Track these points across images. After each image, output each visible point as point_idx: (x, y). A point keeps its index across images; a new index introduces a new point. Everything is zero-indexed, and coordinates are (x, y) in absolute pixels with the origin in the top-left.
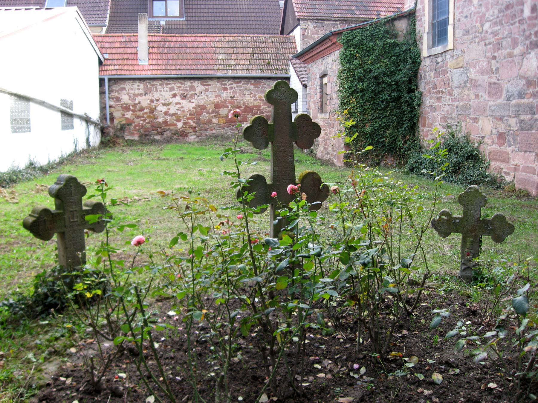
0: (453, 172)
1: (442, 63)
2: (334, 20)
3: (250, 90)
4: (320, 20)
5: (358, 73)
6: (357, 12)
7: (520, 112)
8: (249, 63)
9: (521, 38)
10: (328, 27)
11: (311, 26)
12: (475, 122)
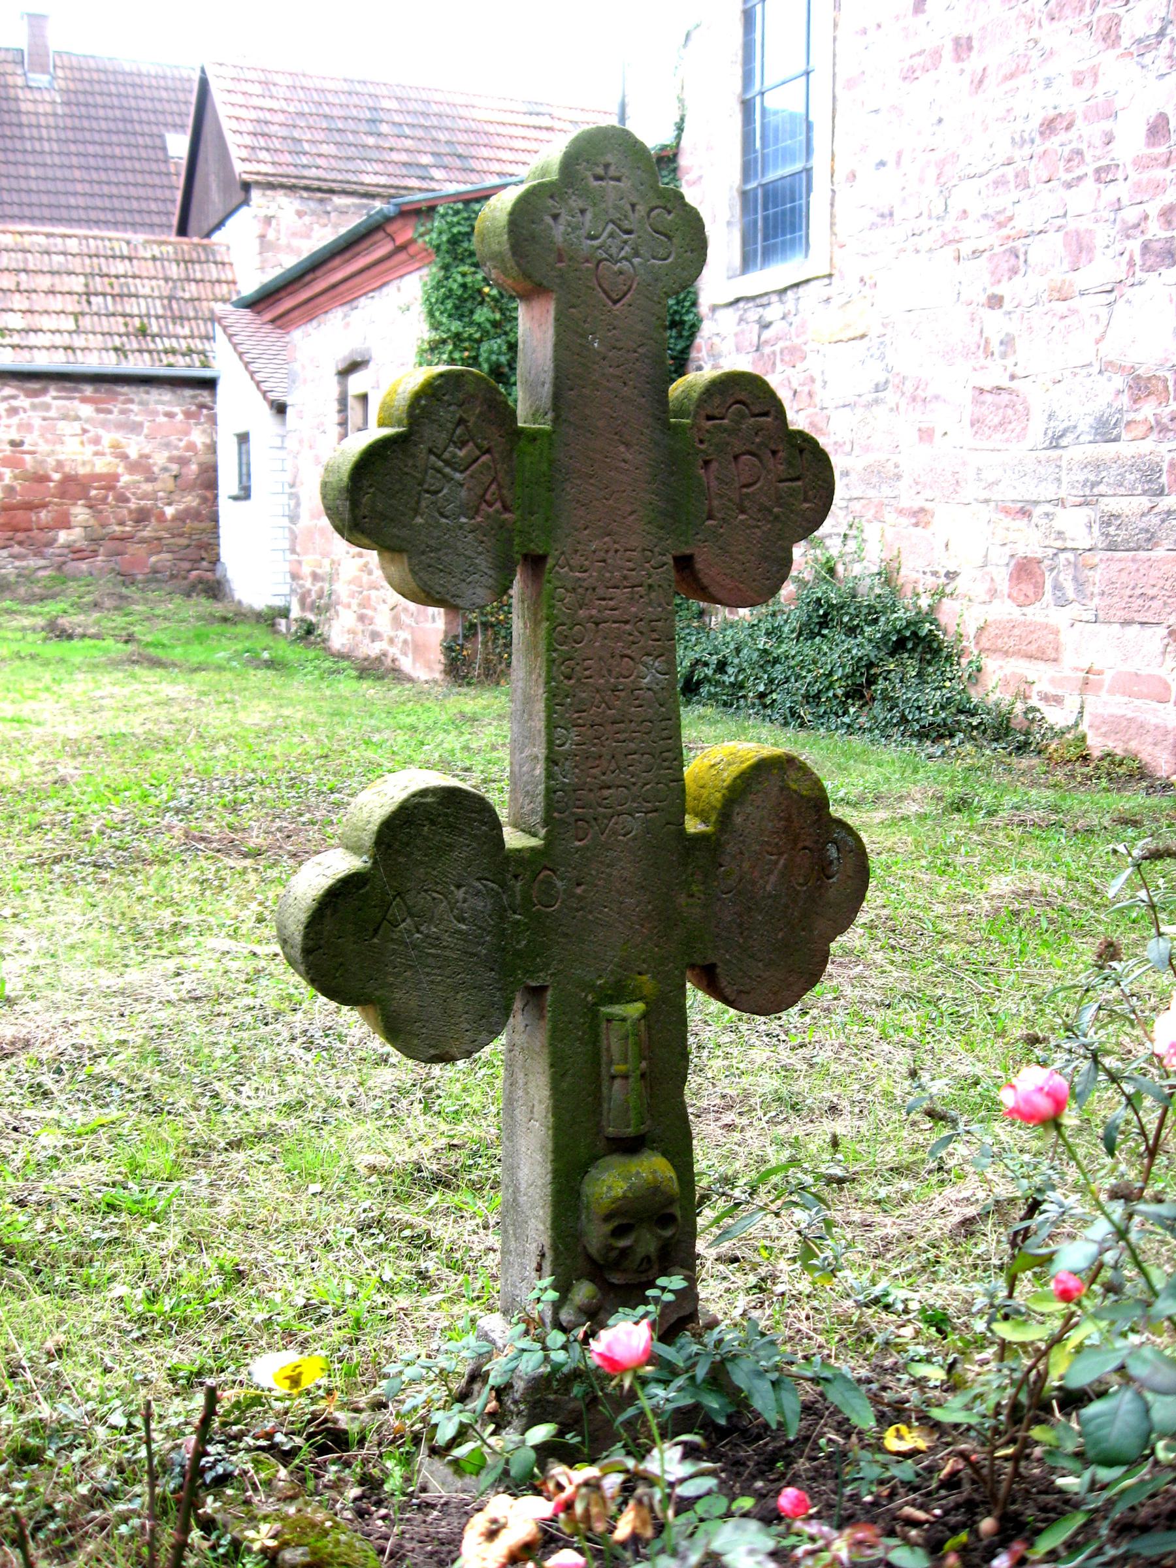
0: (847, 695)
1: (784, 323)
2: (366, 195)
3: (77, 418)
4: (319, 190)
5: (491, 352)
6: (438, 174)
7: (1102, 489)
8: (73, 327)
9: (1102, 234)
10: (344, 217)
11: (285, 206)
12: (916, 525)
